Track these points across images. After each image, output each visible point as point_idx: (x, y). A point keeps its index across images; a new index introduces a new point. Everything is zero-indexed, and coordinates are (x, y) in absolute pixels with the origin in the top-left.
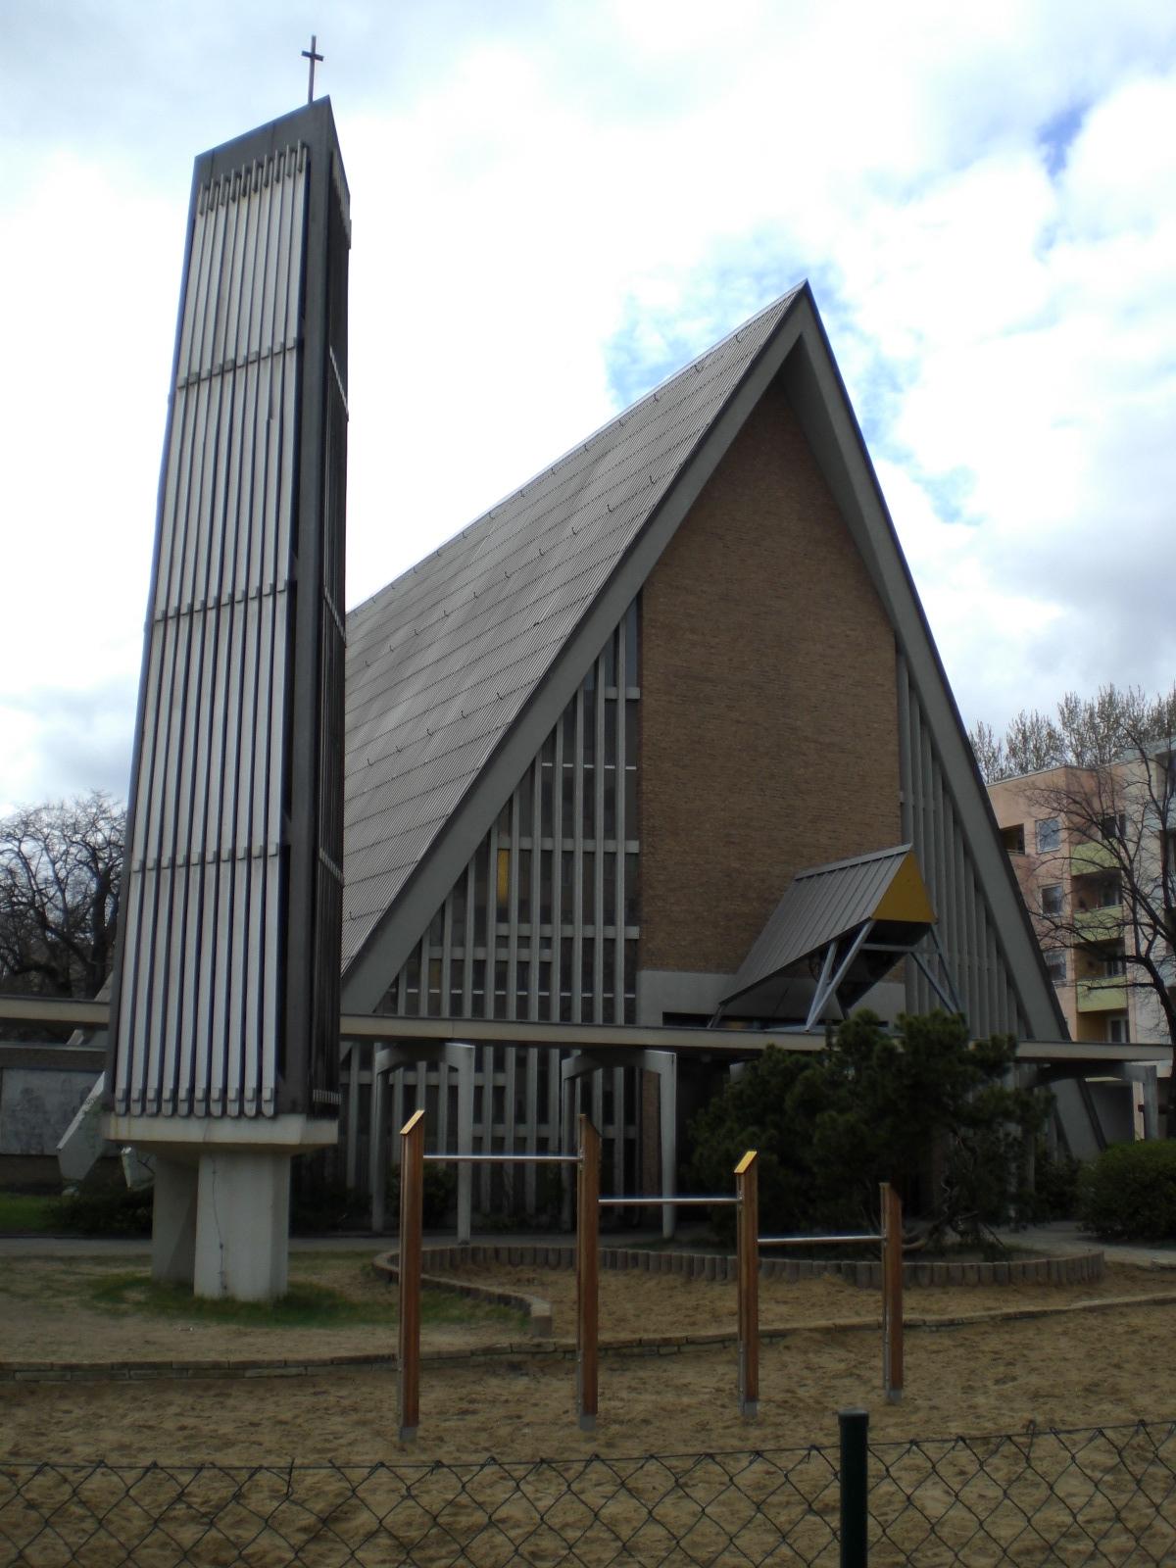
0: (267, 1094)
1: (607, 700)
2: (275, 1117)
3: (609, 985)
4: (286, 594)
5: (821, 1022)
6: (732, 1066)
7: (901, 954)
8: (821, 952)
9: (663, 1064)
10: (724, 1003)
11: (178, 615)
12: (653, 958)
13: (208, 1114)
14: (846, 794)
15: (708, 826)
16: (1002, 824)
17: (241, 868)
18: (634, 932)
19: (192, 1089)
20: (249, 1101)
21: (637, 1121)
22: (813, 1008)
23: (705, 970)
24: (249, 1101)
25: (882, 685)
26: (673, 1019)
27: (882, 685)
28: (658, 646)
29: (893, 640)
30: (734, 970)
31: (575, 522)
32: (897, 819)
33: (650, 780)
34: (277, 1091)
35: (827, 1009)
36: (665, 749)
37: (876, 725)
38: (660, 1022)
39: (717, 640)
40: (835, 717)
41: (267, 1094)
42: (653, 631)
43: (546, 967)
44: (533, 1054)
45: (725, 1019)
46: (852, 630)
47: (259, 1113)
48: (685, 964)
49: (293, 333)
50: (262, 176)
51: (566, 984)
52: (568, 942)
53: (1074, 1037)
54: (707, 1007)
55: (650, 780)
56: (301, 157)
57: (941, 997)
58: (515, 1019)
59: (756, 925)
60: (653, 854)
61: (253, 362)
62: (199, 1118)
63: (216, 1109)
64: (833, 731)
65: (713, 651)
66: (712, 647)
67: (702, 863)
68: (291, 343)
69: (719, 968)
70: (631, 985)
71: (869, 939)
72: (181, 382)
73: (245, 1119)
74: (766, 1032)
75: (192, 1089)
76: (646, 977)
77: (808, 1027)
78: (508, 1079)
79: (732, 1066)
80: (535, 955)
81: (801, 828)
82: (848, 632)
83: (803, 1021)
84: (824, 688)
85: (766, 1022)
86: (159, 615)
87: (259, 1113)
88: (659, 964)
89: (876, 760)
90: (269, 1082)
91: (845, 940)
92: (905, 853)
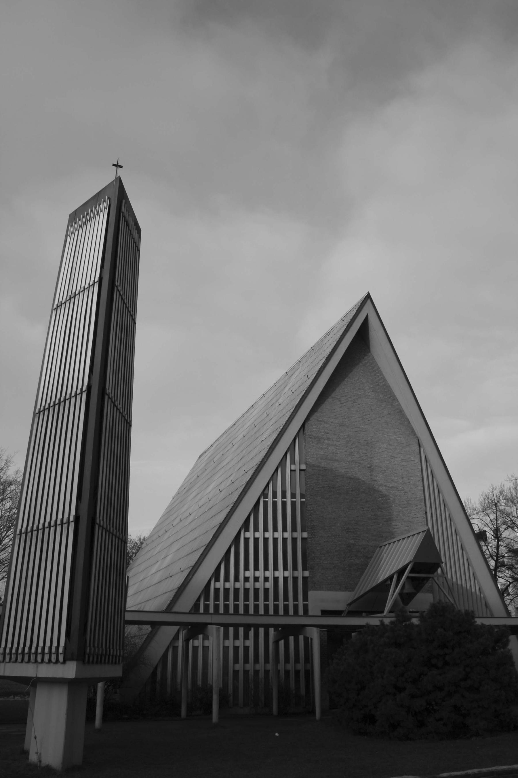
0: (61, 650)
1: (291, 470)
2: (64, 662)
3: (296, 598)
4: (86, 392)
5: (390, 612)
6: (353, 634)
7: (427, 579)
8: (391, 578)
9: (315, 634)
10: (350, 604)
11: (44, 409)
12: (316, 585)
13: (36, 661)
14: (400, 509)
15: (338, 524)
16: (476, 529)
17: (59, 528)
18: (307, 574)
19: (44, 648)
20: (53, 654)
21: (310, 662)
22: (387, 604)
23: (340, 590)
24: (53, 654)
25: (414, 461)
26: (325, 613)
27: (414, 461)
28: (313, 446)
29: (418, 441)
30: (353, 590)
31: (280, 401)
32: (423, 519)
33: (311, 505)
34: (65, 648)
35: (395, 604)
36: (318, 491)
37: (412, 478)
38: (320, 614)
39: (339, 443)
40: (393, 475)
41: (61, 650)
42: (311, 440)
43: (266, 590)
44: (262, 630)
45: (351, 613)
46: (398, 437)
47: (57, 661)
48: (331, 588)
49: (98, 275)
50: (92, 213)
51: (276, 598)
52: (276, 579)
53: (513, 614)
54: (341, 607)
55: (311, 505)
56: (107, 202)
57: (444, 594)
58: (242, 613)
59: (362, 569)
60: (314, 538)
61: (82, 291)
62: (33, 663)
63: (39, 659)
64: (392, 481)
65: (338, 448)
66: (337, 446)
67: (337, 541)
68: (97, 280)
69: (346, 589)
70: (305, 598)
71: (411, 572)
72: (55, 307)
73: (52, 663)
74: (368, 617)
75: (44, 648)
76: (311, 594)
77: (385, 614)
78: (250, 643)
79: (353, 634)
80: (260, 585)
81: (381, 525)
82: (397, 438)
83: (383, 612)
84: (388, 462)
85: (370, 613)
86: (37, 411)
87: (57, 661)
88: (318, 587)
89: (413, 493)
90: (62, 643)
91: (401, 572)
92: (425, 531)
